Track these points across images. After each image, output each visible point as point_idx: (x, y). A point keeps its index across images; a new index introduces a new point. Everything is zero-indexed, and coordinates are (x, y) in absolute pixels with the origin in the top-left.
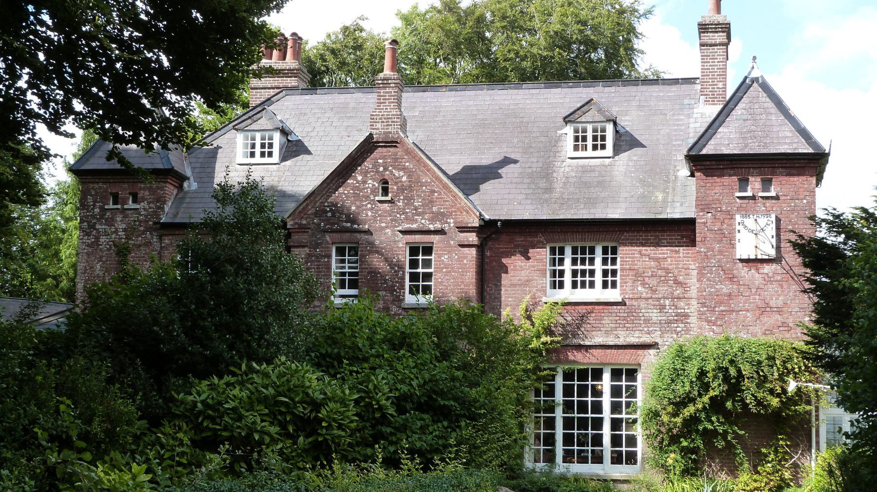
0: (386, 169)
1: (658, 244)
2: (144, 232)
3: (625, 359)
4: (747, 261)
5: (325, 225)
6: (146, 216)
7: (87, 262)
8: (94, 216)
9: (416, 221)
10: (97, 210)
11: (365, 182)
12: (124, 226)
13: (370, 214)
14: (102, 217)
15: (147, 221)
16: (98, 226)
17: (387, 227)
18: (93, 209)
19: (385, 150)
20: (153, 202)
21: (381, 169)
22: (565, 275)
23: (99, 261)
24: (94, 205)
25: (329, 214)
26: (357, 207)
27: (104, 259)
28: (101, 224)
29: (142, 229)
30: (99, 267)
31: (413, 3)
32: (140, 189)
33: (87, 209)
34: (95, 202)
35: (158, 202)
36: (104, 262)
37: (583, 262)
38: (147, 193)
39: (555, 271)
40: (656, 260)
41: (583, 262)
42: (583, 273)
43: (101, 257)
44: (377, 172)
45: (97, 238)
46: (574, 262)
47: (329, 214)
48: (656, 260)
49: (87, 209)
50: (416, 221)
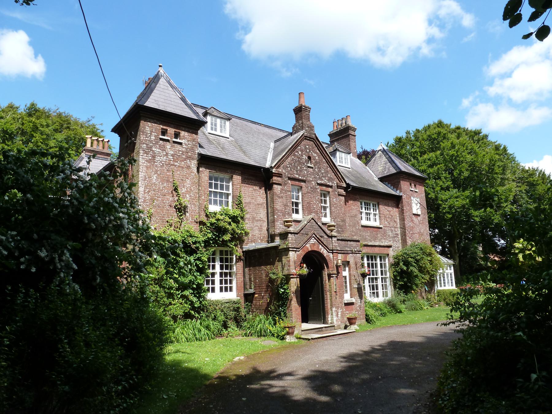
0: (310, 151)
1: (389, 206)
2: (185, 159)
3: (384, 251)
4: (414, 214)
6: (186, 149)
7: (146, 172)
8: (151, 141)
10: (153, 138)
11: (302, 156)
12: (172, 153)
15: (188, 153)
18: (150, 136)
19: (309, 141)
20: (191, 141)
22: (216, 276)
23: (155, 174)
24: (151, 134)
25: (289, 169)
26: (300, 168)
27: (159, 173)
28: (155, 148)
29: (184, 157)
30: (155, 178)
31: (530, 22)
33: (146, 135)
34: (151, 132)
35: (193, 141)
36: (159, 175)
37: (227, 269)
40: (389, 211)
42: (226, 274)
43: (157, 171)
44: (307, 152)
45: (154, 157)
46: (222, 268)
47: (289, 169)
48: (389, 211)
49: (146, 135)
50: (322, 180)
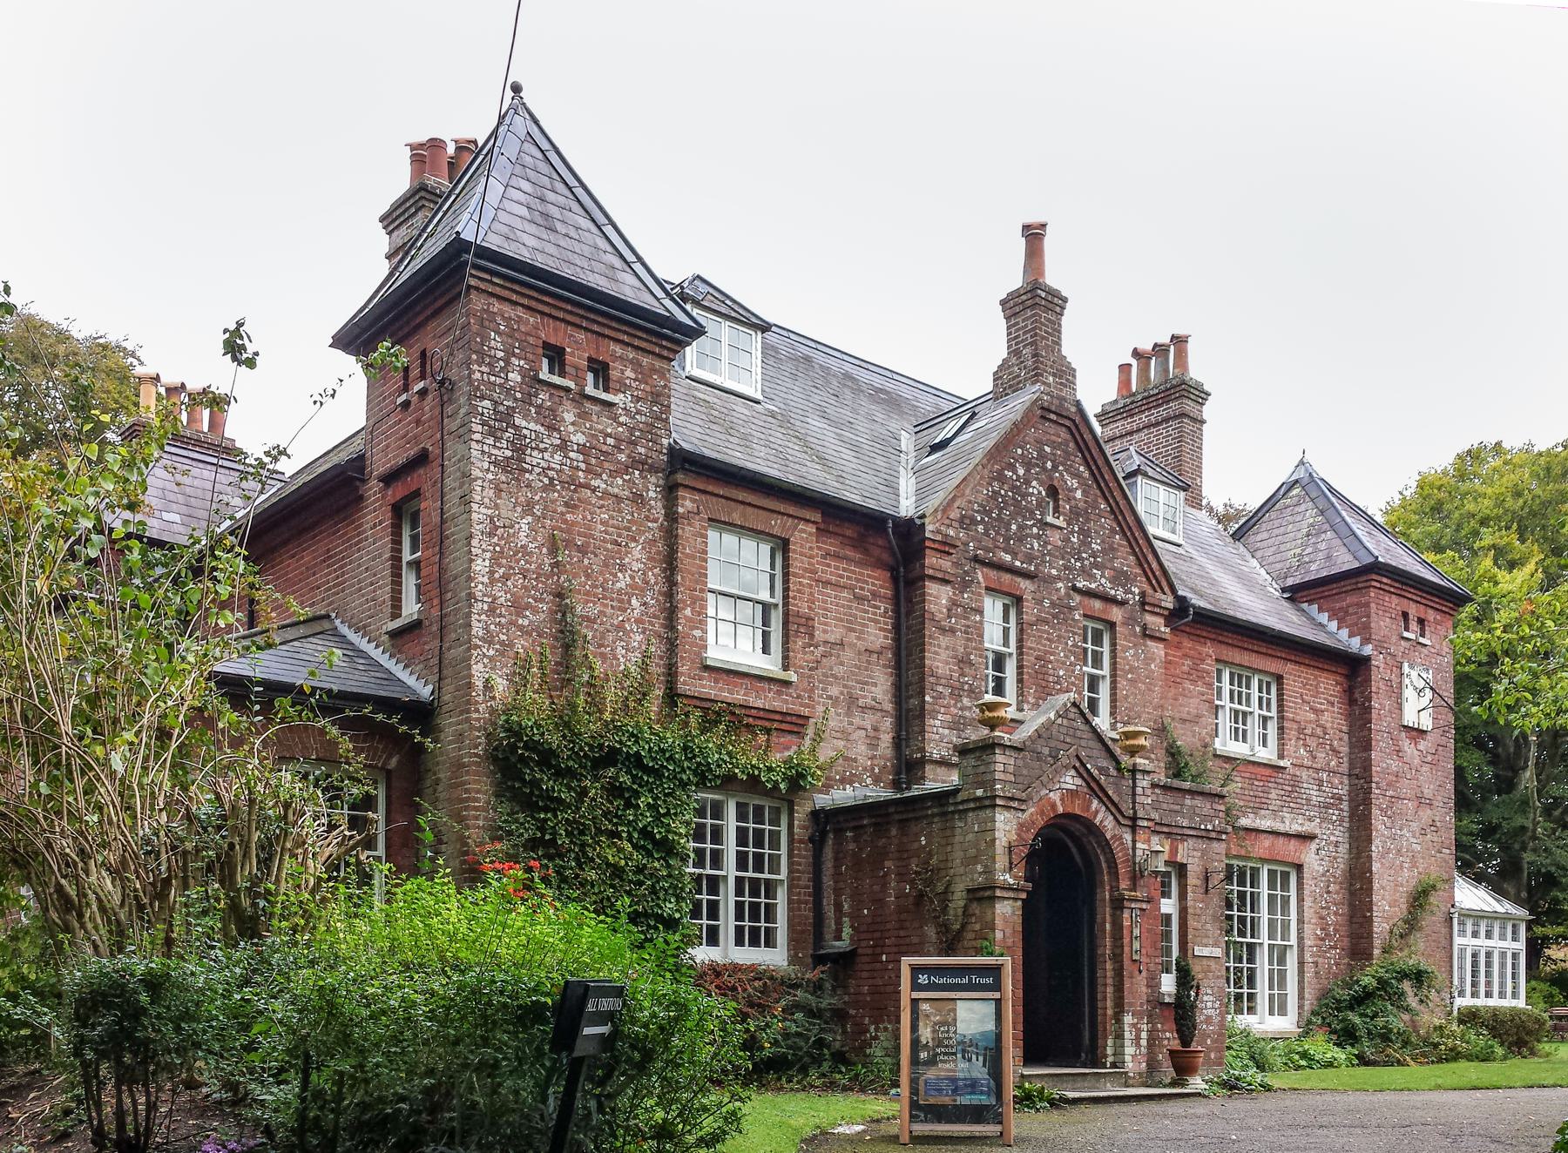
0: (1055, 468)
5: (976, 548)
9: (1092, 577)
13: (1036, 546)
14: (528, 399)
15: (634, 444)
16: (519, 421)
17: (1059, 578)
18: (505, 370)
21: (1049, 465)
25: (980, 528)
30: (525, 527)
31: (1041, 220)
32: (615, 358)
34: (510, 353)
38: (629, 373)
39: (1236, 712)
41: (759, 867)
42: (755, 883)
44: (1044, 469)
